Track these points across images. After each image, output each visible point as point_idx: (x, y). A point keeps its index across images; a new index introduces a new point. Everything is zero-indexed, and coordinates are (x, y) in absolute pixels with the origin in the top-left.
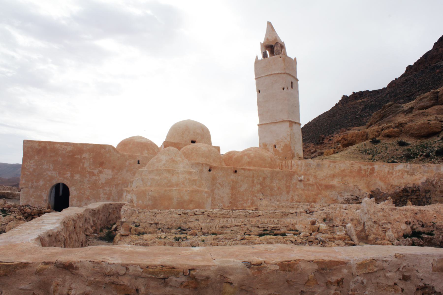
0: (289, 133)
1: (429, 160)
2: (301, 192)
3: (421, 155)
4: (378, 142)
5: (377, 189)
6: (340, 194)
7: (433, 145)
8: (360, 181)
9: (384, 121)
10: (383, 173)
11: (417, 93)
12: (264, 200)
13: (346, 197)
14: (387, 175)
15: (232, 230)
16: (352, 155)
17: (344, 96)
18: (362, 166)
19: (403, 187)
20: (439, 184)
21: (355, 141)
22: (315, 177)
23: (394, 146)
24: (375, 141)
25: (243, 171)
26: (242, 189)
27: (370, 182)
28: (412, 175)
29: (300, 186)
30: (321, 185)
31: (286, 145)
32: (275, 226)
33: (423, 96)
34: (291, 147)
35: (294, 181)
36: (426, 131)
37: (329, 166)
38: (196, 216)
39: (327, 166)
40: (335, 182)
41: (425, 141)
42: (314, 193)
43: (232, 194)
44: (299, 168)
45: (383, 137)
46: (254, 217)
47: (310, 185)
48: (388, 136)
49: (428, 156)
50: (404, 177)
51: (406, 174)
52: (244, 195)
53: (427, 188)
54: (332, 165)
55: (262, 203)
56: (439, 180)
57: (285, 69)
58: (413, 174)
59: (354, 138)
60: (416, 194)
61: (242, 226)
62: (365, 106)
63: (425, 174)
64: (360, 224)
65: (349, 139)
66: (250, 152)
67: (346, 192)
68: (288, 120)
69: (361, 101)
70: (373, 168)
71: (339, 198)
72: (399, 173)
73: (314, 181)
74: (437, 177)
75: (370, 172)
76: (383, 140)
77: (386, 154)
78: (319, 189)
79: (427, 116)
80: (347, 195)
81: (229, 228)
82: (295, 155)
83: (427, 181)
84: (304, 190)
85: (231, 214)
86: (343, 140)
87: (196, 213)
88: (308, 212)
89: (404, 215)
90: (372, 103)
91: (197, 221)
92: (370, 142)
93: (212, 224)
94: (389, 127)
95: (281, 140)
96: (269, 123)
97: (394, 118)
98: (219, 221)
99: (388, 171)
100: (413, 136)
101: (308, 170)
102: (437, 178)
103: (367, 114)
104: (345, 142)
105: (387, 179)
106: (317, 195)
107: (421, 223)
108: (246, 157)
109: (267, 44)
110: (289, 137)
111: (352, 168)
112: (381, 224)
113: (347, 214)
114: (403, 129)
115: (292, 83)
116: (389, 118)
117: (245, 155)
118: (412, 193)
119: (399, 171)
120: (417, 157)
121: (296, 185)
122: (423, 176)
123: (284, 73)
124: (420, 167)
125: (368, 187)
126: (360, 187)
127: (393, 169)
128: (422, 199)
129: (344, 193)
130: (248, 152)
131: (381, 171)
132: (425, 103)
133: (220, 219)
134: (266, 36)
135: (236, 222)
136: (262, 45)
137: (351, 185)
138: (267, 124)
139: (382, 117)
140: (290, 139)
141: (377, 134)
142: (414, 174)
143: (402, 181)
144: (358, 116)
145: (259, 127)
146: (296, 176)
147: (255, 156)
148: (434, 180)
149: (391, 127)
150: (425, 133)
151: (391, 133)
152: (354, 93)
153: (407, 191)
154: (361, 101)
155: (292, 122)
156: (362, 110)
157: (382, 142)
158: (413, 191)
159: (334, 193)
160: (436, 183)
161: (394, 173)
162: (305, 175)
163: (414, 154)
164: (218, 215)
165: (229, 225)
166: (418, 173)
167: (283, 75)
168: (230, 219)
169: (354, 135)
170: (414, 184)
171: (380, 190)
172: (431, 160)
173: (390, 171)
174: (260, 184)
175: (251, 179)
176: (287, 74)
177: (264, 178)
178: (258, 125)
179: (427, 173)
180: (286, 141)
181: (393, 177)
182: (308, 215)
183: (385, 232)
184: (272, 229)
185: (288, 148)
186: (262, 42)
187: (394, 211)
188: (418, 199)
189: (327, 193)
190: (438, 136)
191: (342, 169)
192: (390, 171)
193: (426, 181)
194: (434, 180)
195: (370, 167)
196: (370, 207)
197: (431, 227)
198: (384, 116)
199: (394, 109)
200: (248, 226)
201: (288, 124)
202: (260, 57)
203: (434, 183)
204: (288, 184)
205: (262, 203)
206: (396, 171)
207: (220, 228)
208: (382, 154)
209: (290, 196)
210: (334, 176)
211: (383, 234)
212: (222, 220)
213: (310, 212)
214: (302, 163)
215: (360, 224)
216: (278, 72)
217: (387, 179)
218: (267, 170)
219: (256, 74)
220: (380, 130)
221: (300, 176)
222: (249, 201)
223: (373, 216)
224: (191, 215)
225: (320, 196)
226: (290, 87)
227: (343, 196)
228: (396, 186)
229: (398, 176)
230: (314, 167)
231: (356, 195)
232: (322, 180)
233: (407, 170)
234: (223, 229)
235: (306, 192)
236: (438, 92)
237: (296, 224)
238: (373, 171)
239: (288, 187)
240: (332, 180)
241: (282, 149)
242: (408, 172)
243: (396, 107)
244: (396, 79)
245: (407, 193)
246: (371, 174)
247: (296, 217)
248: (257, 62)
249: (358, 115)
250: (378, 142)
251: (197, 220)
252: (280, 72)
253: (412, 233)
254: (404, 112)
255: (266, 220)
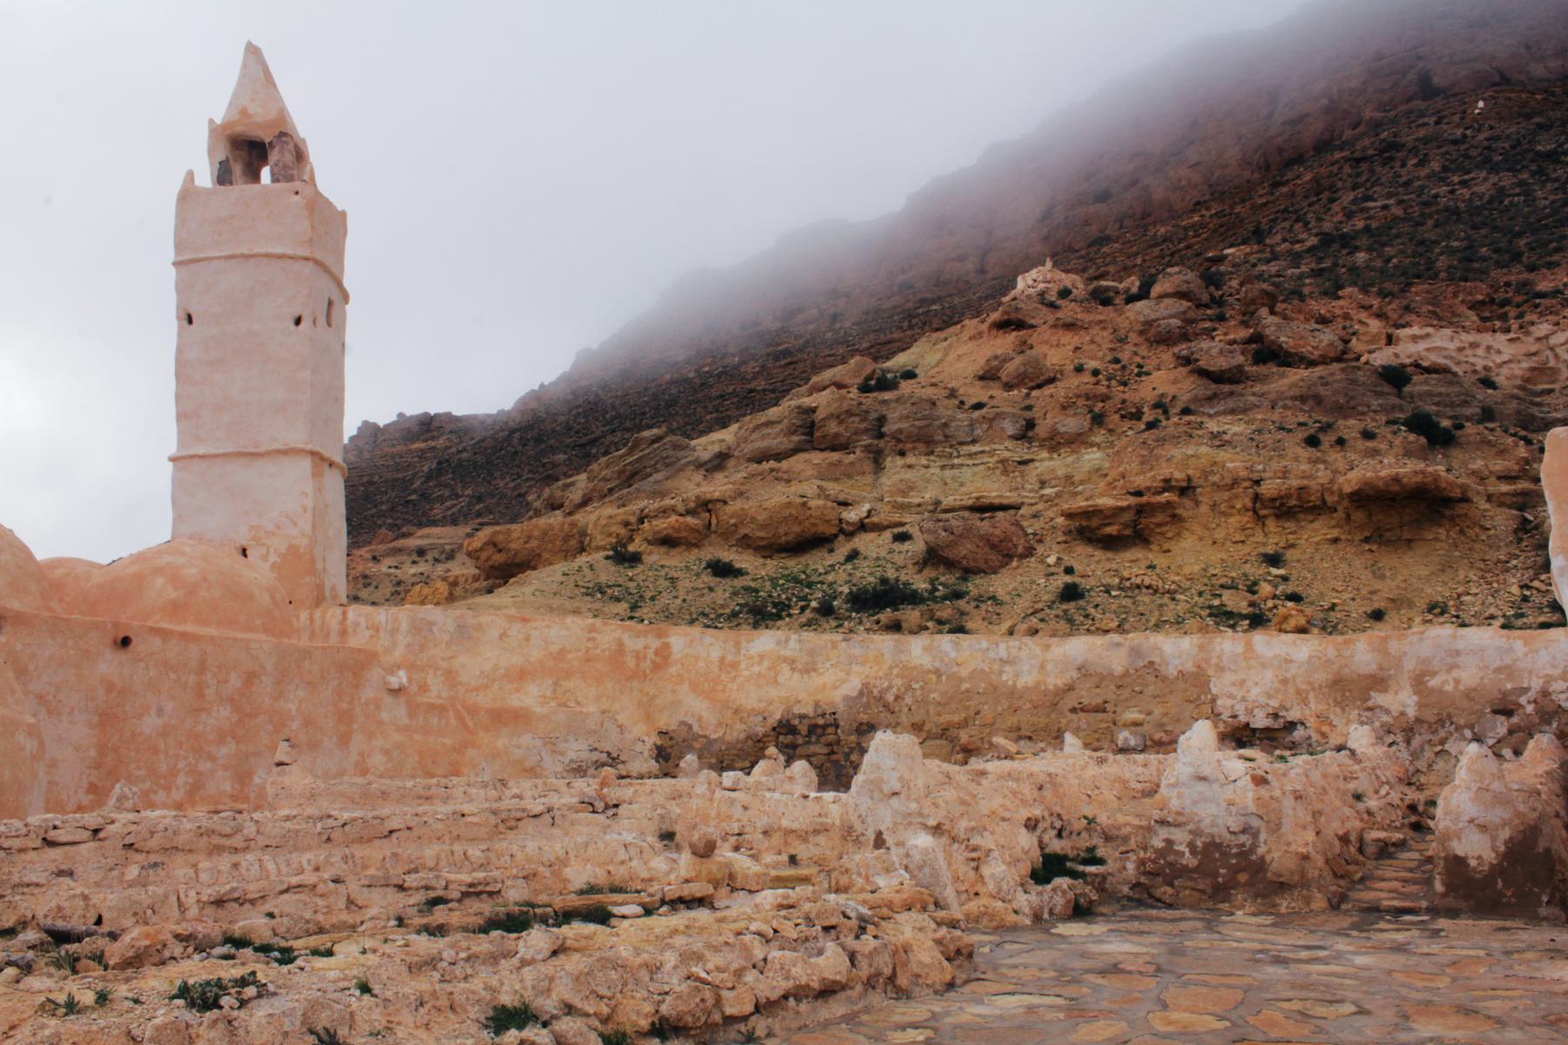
0: (309, 503)
1: (834, 623)
2: (397, 737)
3: (803, 609)
4: (635, 559)
5: (683, 723)
6: (551, 743)
7: (830, 578)
8: (622, 692)
9: (638, 490)
10: (701, 664)
11: (609, 438)
12: (294, 768)
13: (572, 755)
14: (716, 670)
15: (271, 915)
16: (556, 602)
17: (366, 423)
18: (626, 639)
19: (778, 716)
20: (908, 700)
21: (539, 555)
22: (451, 677)
23: (698, 575)
24: (624, 557)
25: (156, 642)
26: (149, 724)
27: (653, 698)
28: (807, 671)
29: (395, 712)
30: (473, 710)
31: (293, 551)
32: (480, 875)
33: (763, 420)
34: (313, 561)
35: (368, 693)
36: (797, 529)
37: (503, 636)
38: (54, 853)
39: (495, 633)
40: (530, 697)
41: (791, 563)
42: (448, 741)
43: (102, 749)
44: (384, 640)
45: (650, 543)
46: (370, 840)
47: (432, 707)
48: (667, 542)
49: (826, 610)
50: (781, 679)
51: (785, 668)
52: (157, 752)
53: (864, 718)
54: (516, 630)
55: (286, 780)
56: (909, 688)
57: (311, 241)
58: (810, 669)
59: (534, 544)
60: (823, 739)
61: (321, 888)
62: (439, 463)
63: (856, 668)
64: (857, 841)
65: (513, 546)
66: (181, 560)
67: (571, 738)
68: (309, 447)
69: (423, 445)
70: (667, 646)
71: (547, 758)
72: (760, 663)
73: (444, 694)
74: (898, 676)
75: (653, 662)
76: (650, 553)
77: (678, 601)
78: (467, 728)
79: (788, 481)
80: (577, 749)
81: (253, 902)
82: (327, 594)
83: (865, 691)
84: (406, 729)
85: (250, 829)
86: (491, 550)
87: (52, 835)
88: (600, 805)
89: (1014, 793)
90: (464, 455)
91: (67, 880)
92: (607, 558)
93: (161, 891)
94: (665, 512)
95: (271, 527)
96: (225, 455)
97: (670, 484)
98: (191, 872)
99: (722, 660)
100: (748, 547)
101: (423, 648)
102: (899, 682)
103: (447, 493)
104: (499, 558)
105: (720, 687)
106: (460, 749)
107: (1058, 824)
108: (160, 581)
109: (239, 129)
110: (309, 515)
111: (590, 645)
112: (962, 836)
113: (745, 808)
114: (714, 521)
115: (330, 303)
116: (656, 482)
117: (158, 571)
118: (809, 735)
119: (762, 657)
120: (790, 615)
121: (378, 708)
122: (848, 673)
123: (306, 259)
124: (834, 645)
125: (648, 717)
126: (621, 718)
127: (738, 651)
128: (847, 756)
129: (566, 741)
130: (167, 559)
131: (697, 658)
132: (774, 440)
133: (192, 858)
134: (236, 95)
135: (284, 869)
136: (215, 131)
137: (592, 708)
138: (216, 456)
139: (630, 477)
140: (314, 527)
141: (623, 531)
142: (815, 670)
143: (773, 693)
144: (414, 497)
145: (176, 470)
146: (375, 674)
147: (205, 579)
148: (890, 687)
149: (673, 510)
150: (790, 537)
151: (678, 530)
152: (401, 415)
153: (792, 730)
154: (423, 445)
155: (323, 459)
156: (429, 477)
157: (649, 559)
158: (813, 728)
159: (526, 739)
160: (897, 698)
161: (743, 666)
162: (411, 667)
163: (775, 605)
164: (180, 841)
165: (253, 889)
166: (828, 665)
167: (299, 266)
168: (250, 857)
169: (536, 533)
170: (817, 704)
171: (696, 729)
172: (840, 626)
173: (729, 658)
174: (231, 700)
175: (192, 679)
176: (317, 262)
177: (251, 677)
178: (173, 459)
179: (863, 664)
180: (294, 532)
181: (740, 680)
182: (601, 818)
183: (977, 863)
184: (465, 895)
185: (298, 562)
186: (218, 121)
187: (984, 782)
188: (834, 757)
189: (501, 743)
190: (831, 551)
191: (555, 648)
192: (729, 658)
193: (861, 693)
194: (890, 687)
195: (655, 644)
196: (912, 770)
197: (1084, 834)
198: (635, 474)
199: (671, 452)
200: (353, 887)
201: (306, 464)
202: (205, 178)
203: (890, 698)
204: (345, 706)
205: (286, 780)
206: (751, 658)
207: (209, 910)
208: (665, 599)
209: (354, 757)
210: (522, 675)
211: (972, 874)
212: (204, 864)
213: (607, 807)
214: (396, 620)
215: (857, 841)
216: (279, 250)
217: (720, 687)
218: (262, 642)
219: (179, 245)
220: (633, 520)
221: (392, 670)
222: (181, 779)
223: (928, 802)
224: (21, 850)
225: (472, 753)
226: (322, 320)
227: (562, 754)
228: (754, 712)
229: (759, 675)
230: (446, 637)
231: (608, 748)
232: (477, 689)
233: (788, 653)
234: (222, 913)
235: (418, 737)
236: (814, 410)
237: (564, 862)
238: (666, 658)
239: (344, 718)
240: (518, 691)
241: (274, 565)
242: (792, 662)
243: (676, 447)
244: (542, 386)
245: (790, 738)
246: (656, 667)
247: (556, 831)
248: (188, 194)
249: (415, 491)
250: (635, 559)
251: (61, 873)
252: (290, 252)
253: (1044, 863)
254: (699, 465)
255: (429, 853)
